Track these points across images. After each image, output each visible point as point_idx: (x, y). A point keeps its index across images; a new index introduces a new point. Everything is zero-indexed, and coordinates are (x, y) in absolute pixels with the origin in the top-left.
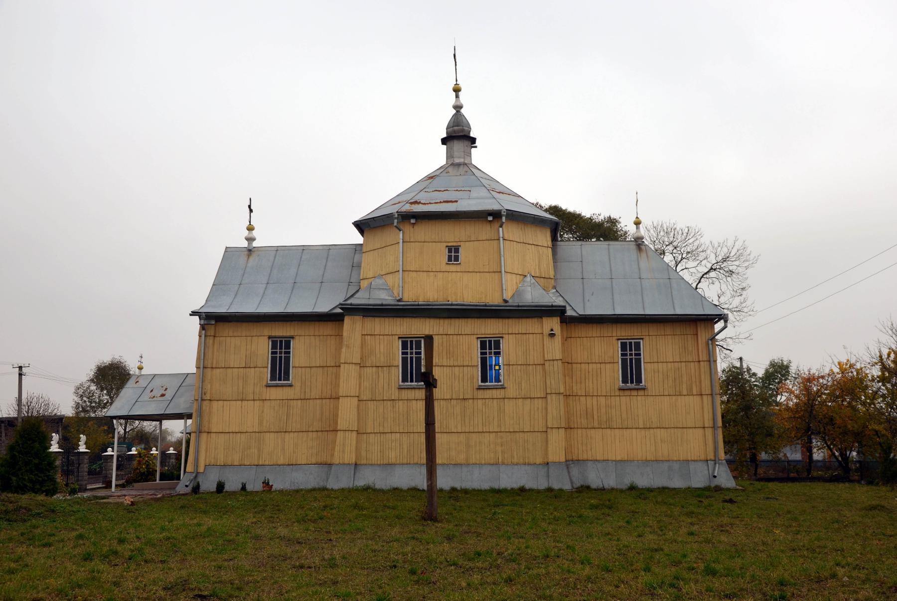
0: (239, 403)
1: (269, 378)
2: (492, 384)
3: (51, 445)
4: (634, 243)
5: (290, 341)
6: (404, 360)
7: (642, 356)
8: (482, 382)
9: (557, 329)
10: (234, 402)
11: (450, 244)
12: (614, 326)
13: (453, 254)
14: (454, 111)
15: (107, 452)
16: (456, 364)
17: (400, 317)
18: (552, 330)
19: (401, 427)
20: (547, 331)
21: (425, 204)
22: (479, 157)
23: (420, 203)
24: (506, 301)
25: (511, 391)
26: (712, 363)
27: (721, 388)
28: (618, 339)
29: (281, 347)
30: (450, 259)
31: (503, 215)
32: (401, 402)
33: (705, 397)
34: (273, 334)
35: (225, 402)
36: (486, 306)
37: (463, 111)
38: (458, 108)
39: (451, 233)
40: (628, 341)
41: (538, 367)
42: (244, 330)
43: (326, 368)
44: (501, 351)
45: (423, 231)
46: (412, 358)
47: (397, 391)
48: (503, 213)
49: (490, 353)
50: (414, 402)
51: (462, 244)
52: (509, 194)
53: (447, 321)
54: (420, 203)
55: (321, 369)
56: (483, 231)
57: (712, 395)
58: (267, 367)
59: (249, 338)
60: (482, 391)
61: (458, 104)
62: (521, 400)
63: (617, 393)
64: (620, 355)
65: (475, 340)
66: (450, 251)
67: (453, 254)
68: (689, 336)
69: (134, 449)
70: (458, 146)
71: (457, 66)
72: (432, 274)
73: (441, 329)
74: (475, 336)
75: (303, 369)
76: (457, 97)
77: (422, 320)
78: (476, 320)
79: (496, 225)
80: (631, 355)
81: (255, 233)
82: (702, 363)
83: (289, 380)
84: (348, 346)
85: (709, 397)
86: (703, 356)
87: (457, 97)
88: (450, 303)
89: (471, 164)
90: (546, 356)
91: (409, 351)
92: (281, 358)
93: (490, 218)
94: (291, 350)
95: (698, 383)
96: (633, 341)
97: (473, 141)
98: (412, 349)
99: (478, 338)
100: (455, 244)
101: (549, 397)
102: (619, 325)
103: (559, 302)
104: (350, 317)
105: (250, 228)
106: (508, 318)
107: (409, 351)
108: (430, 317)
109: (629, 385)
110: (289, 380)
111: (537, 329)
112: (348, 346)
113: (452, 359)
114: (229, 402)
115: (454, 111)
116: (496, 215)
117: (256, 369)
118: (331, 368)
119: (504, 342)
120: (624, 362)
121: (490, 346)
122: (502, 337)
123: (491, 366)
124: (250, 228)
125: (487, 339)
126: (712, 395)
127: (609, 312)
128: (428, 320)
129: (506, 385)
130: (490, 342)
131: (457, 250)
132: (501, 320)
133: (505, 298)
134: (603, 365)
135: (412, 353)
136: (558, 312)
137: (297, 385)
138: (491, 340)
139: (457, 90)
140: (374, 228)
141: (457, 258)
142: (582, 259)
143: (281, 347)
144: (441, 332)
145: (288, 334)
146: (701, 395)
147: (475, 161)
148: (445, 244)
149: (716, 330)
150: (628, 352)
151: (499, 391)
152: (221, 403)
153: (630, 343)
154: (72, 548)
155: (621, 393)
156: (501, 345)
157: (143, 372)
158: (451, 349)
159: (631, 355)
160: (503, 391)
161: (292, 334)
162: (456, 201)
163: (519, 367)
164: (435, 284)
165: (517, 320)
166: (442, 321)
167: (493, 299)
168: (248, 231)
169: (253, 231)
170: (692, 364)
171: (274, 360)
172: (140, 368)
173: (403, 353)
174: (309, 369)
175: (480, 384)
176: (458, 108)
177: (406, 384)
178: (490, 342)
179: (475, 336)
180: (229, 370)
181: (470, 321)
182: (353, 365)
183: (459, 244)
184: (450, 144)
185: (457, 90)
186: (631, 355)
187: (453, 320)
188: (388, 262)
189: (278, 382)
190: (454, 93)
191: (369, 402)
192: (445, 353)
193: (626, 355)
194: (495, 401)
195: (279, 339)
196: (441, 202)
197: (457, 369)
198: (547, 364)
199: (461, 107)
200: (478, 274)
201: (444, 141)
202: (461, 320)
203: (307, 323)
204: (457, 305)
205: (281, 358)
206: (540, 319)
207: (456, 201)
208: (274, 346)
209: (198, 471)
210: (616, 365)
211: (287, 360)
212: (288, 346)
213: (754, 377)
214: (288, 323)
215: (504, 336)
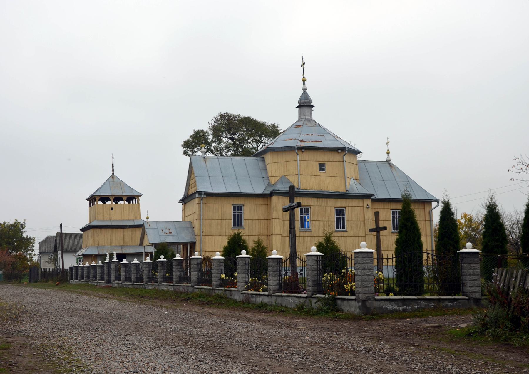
0: (219, 237)
1: (233, 225)
4: (387, 163)
5: (242, 207)
6: (337, 218)
7: (233, 211)
8: (301, 228)
9: (370, 205)
10: (216, 237)
11: (320, 163)
12: (389, 203)
13: (322, 167)
15: (160, 258)
16: (325, 220)
17: (299, 197)
18: (368, 205)
19: (301, 250)
20: (365, 206)
21: (307, 142)
22: (317, 115)
23: (304, 141)
24: (347, 191)
25: (350, 233)
26: (431, 221)
27: (244, 240)
28: (391, 210)
29: (238, 210)
30: (320, 170)
31: (346, 150)
32: (300, 238)
33: (428, 237)
34: (234, 203)
35: (212, 237)
36: (339, 193)
37: (306, 91)
38: (304, 90)
39: (321, 157)
40: (395, 211)
41: (361, 222)
42: (220, 200)
43: (260, 220)
44: (345, 214)
45: (308, 156)
46: (340, 217)
47: (299, 232)
48: (346, 149)
49: (305, 214)
50: (306, 237)
51: (326, 163)
53: (321, 199)
54: (304, 141)
55: (258, 221)
56: (336, 157)
57: (431, 236)
58: (232, 219)
59: (222, 205)
60: (337, 233)
62: (354, 237)
63: (391, 235)
64: (310, 214)
65: (334, 209)
66: (320, 166)
67: (322, 167)
68: (421, 209)
69: (125, 260)
70: (307, 110)
72: (313, 176)
73: (318, 203)
74: (334, 207)
75: (249, 221)
76: (304, 84)
77: (310, 199)
78: (334, 199)
79: (342, 155)
80: (396, 217)
82: (427, 221)
83: (242, 226)
84: (276, 210)
85: (430, 237)
86: (427, 218)
87: (304, 84)
88: (308, 190)
89: (312, 120)
90: (365, 217)
91: (339, 214)
92: (238, 215)
93: (339, 151)
94: (243, 211)
95: (425, 231)
96: (397, 211)
98: (238, 210)
99: (391, 210)
100: (322, 163)
101: (367, 236)
102: (391, 203)
103: (371, 192)
104: (277, 196)
106: (348, 199)
107: (304, 213)
108: (313, 197)
109: (396, 231)
110: (242, 226)
111: (361, 204)
112: (276, 210)
113: (323, 217)
114: (213, 237)
116: (343, 150)
117: (227, 220)
118: (262, 221)
119: (311, 209)
120: (393, 220)
121: (340, 212)
122: (345, 208)
123: (305, 219)
125: (339, 209)
126: (431, 236)
127: (388, 197)
128: (312, 199)
129: (347, 230)
130: (340, 210)
131: (324, 165)
132: (345, 200)
133: (347, 189)
134: (385, 222)
135: (238, 212)
136: (368, 196)
137: (246, 228)
138: (394, 211)
139: (304, 81)
140: (278, 151)
141: (324, 170)
143: (238, 210)
144: (318, 205)
145: (241, 203)
146: (426, 236)
147: (314, 118)
148: (318, 163)
149: (433, 207)
150: (395, 216)
151: (344, 233)
152: (210, 237)
153: (396, 212)
154: (254, 287)
155: (393, 234)
156: (345, 211)
157: (149, 220)
158: (323, 213)
159: (340, 215)
160: (346, 233)
161: (243, 203)
162: (321, 141)
163: (353, 222)
164: (315, 181)
165: (352, 200)
166: (319, 199)
167: (341, 189)
170: (422, 222)
171: (235, 216)
172: (147, 218)
173: (301, 214)
174: (252, 221)
175: (336, 229)
176: (304, 90)
177: (303, 229)
178: (340, 210)
179: (334, 207)
180: (213, 221)
181: (331, 199)
182: (279, 220)
183: (324, 163)
184: (303, 109)
185: (304, 81)
186: (340, 215)
187: (323, 199)
188: (289, 169)
189: (237, 227)
191: (286, 237)
192: (320, 214)
193: (342, 215)
194: (343, 237)
195: (237, 206)
196: (314, 142)
197: (325, 222)
198: (366, 221)
199: (306, 89)
200: (334, 177)
202: (327, 199)
203: (250, 198)
204: (326, 192)
205: (238, 215)
206: (362, 200)
207: (321, 141)
208: (235, 209)
210: (390, 221)
211: (241, 216)
212: (241, 209)
214: (241, 198)
215: (346, 207)
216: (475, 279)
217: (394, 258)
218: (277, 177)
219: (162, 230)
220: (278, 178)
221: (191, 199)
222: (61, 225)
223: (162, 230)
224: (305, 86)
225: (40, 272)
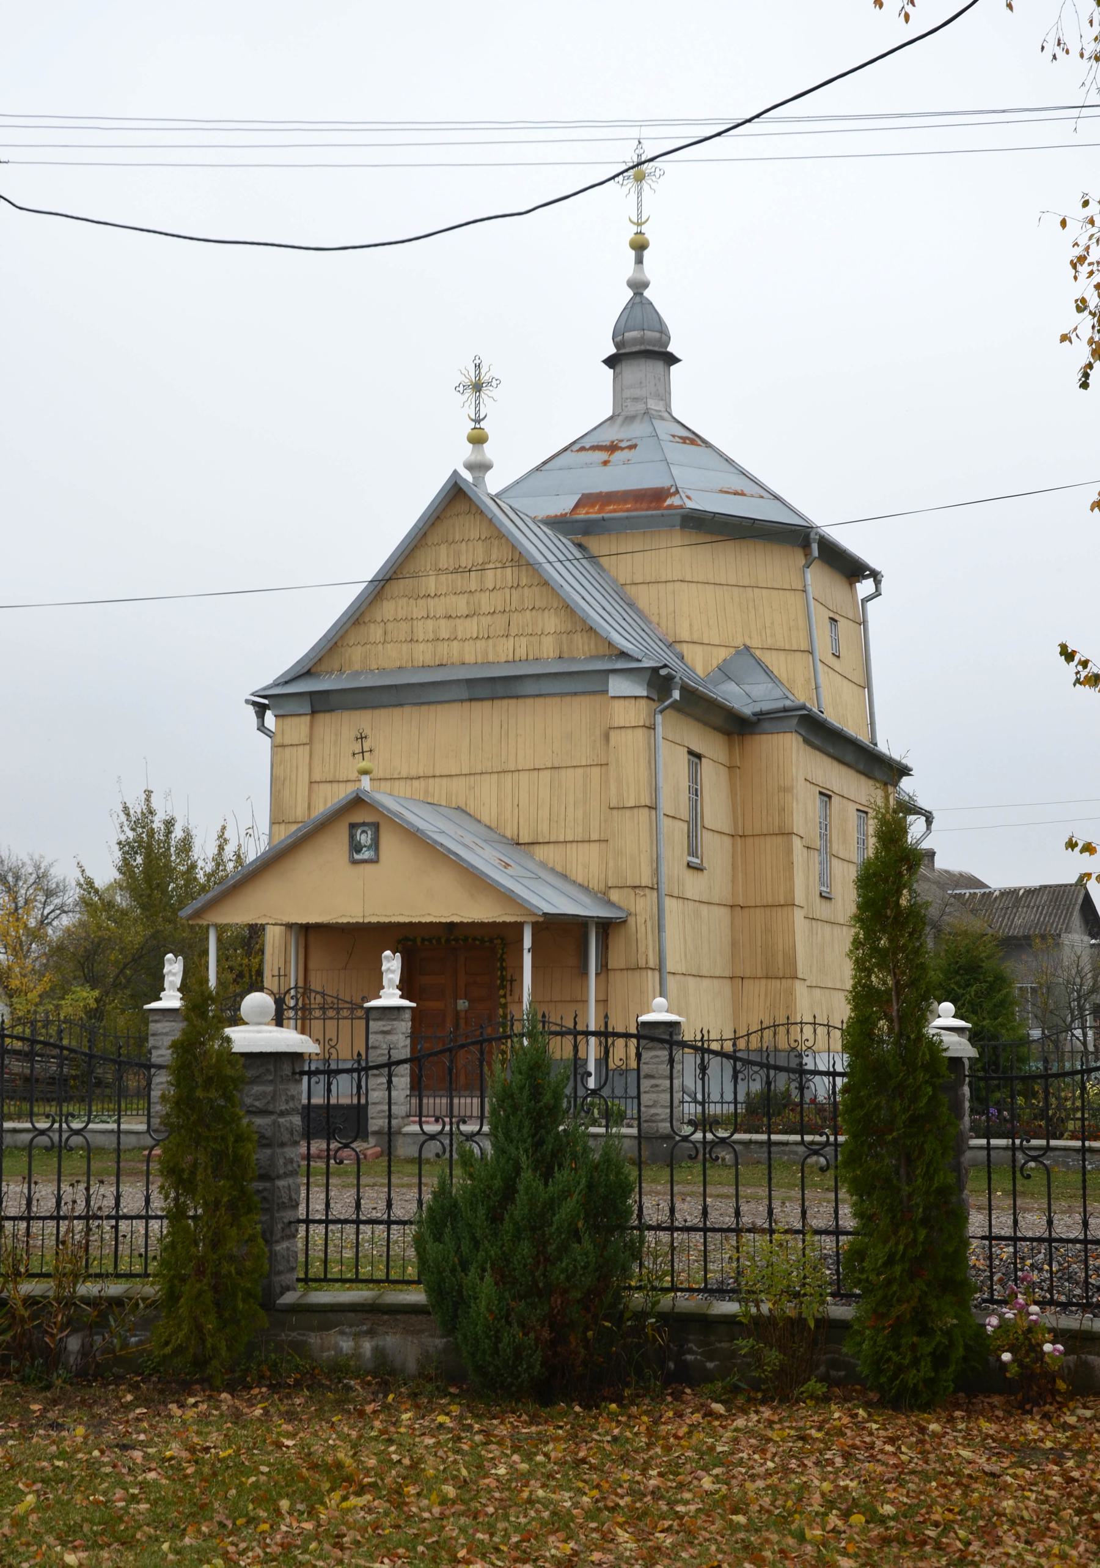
2: (972, 891)
3: (174, 1045)
14: (630, 294)
37: (647, 293)
38: (638, 286)
52: (736, 493)
61: (639, 277)
70: (638, 372)
71: (718, 138)
74: (819, 789)
76: (639, 261)
81: (489, 450)
87: (639, 261)
97: (672, 360)
105: (478, 439)
115: (630, 294)
124: (478, 439)
139: (640, 247)
142: (655, 790)
168: (471, 446)
169: (485, 445)
176: (638, 286)
179: (819, 789)
185: (640, 247)
190: (633, 253)
199: (646, 285)
201: (611, 362)
209: (674, 1047)
213: (409, 1422)
216: (385, 1029)
217: (399, 1063)
218: (715, 650)
219: (1064, 223)
220: (722, 654)
221: (465, 695)
222: (1085, 385)
223: (1064, 223)
224: (642, 270)
225: (173, 843)
